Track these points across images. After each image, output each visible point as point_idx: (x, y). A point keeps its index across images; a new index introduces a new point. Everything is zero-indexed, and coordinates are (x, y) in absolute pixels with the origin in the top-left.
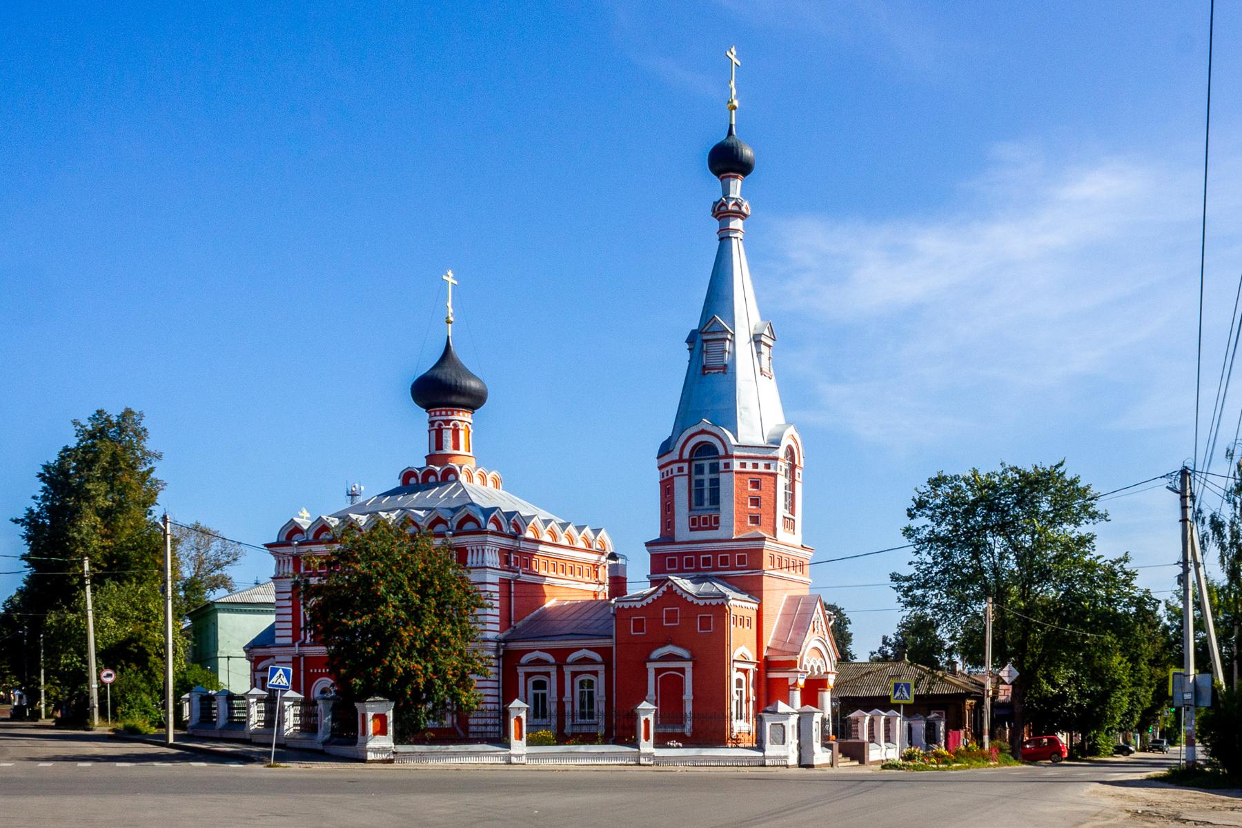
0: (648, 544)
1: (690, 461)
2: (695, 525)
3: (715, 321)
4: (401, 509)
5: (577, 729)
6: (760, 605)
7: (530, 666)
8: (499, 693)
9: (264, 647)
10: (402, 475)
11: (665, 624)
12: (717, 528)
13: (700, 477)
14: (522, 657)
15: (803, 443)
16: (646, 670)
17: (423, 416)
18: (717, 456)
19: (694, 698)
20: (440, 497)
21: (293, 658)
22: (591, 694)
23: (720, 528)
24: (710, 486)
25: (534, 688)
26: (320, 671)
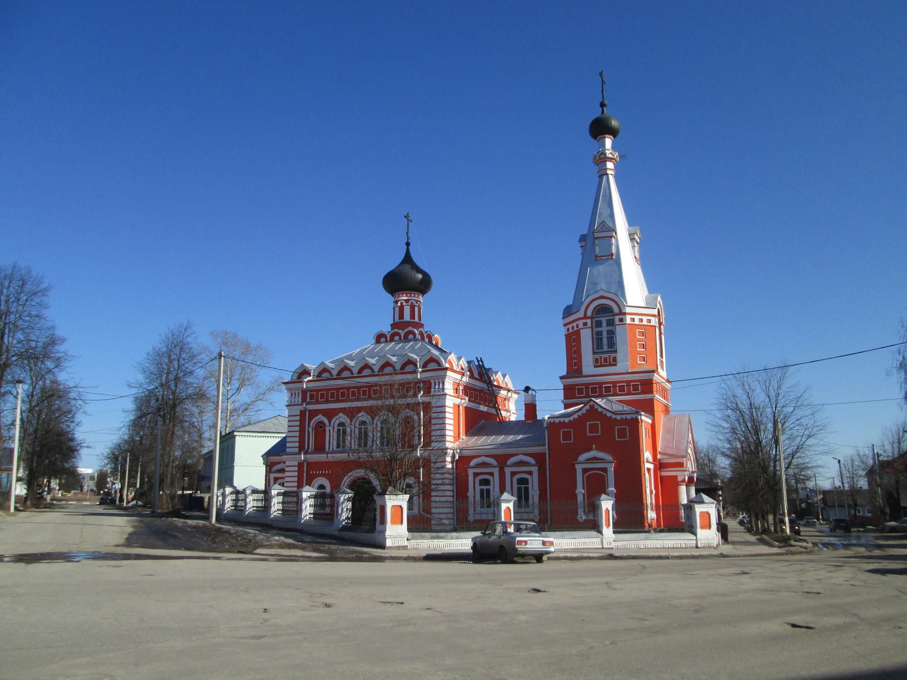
0: (561, 378)
1: (592, 318)
2: (597, 364)
3: (604, 225)
4: (379, 357)
5: (478, 517)
6: (653, 420)
7: (477, 468)
8: (453, 488)
9: (278, 455)
10: (376, 336)
11: (588, 434)
12: (615, 365)
13: (599, 329)
14: (470, 461)
15: (663, 307)
16: (575, 470)
17: (389, 298)
18: (613, 314)
19: (540, 492)
20: (406, 348)
21: (299, 463)
22: (527, 489)
23: (618, 364)
24: (608, 335)
25: (480, 485)
26: (321, 472)
